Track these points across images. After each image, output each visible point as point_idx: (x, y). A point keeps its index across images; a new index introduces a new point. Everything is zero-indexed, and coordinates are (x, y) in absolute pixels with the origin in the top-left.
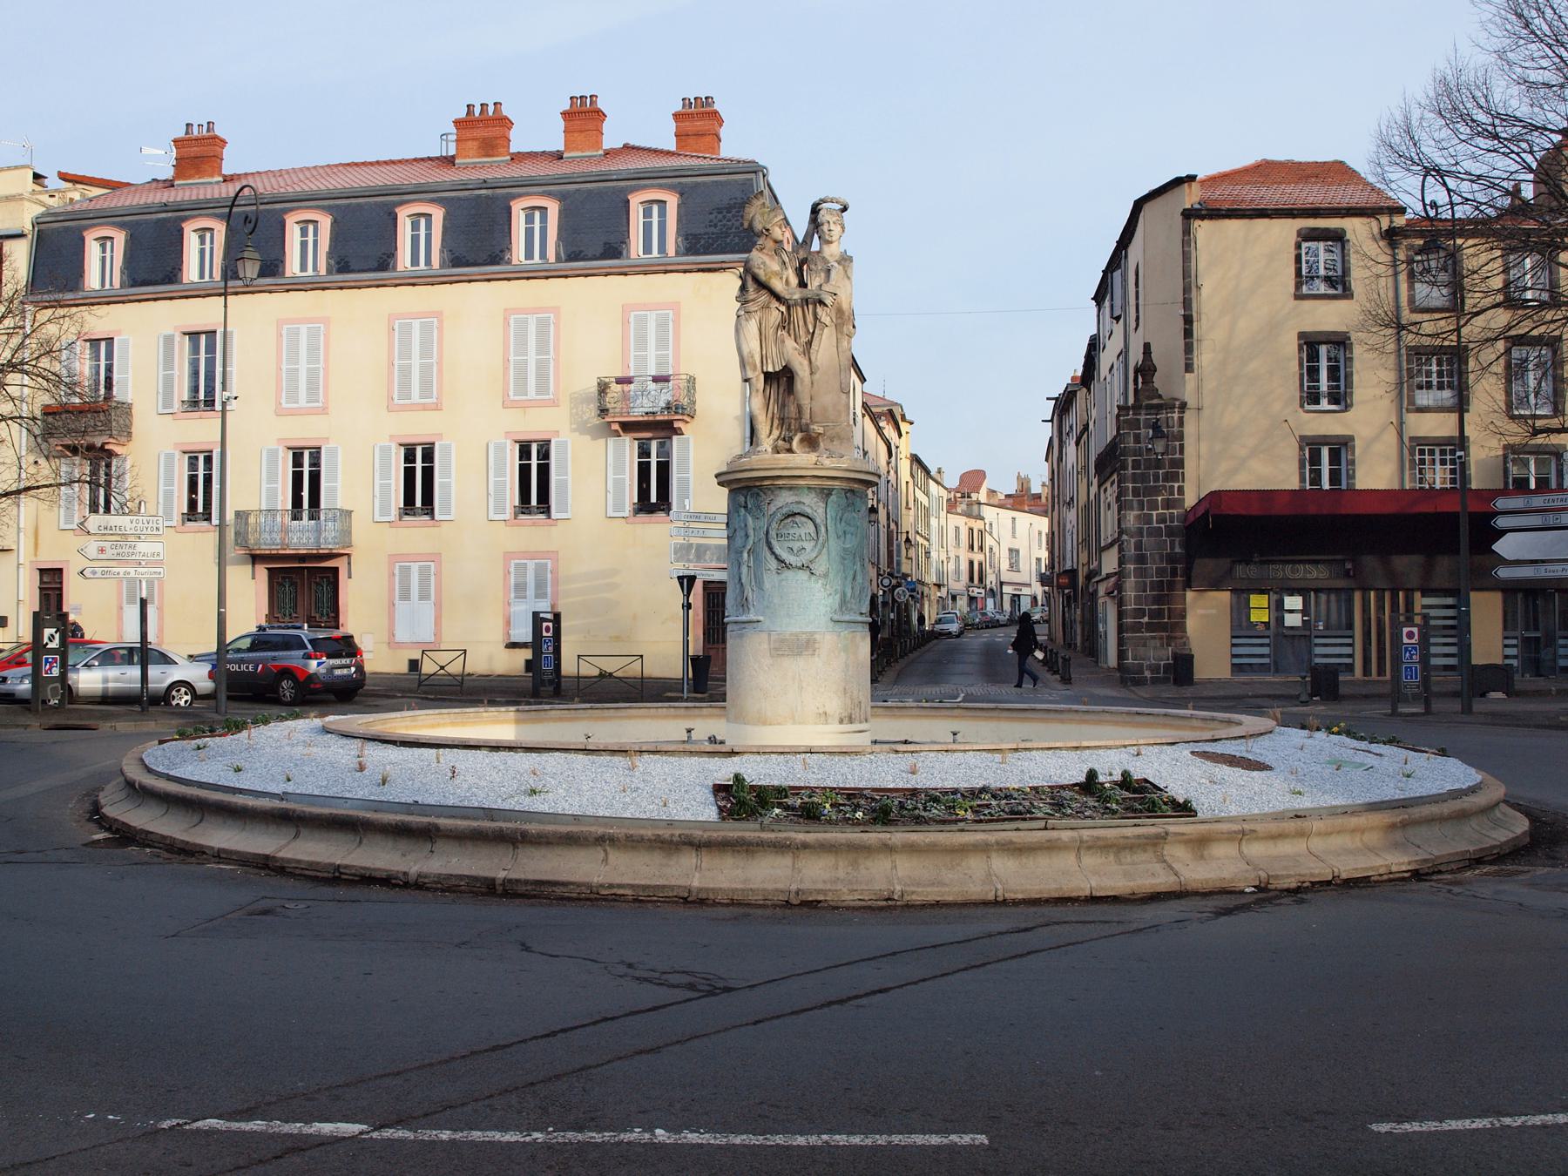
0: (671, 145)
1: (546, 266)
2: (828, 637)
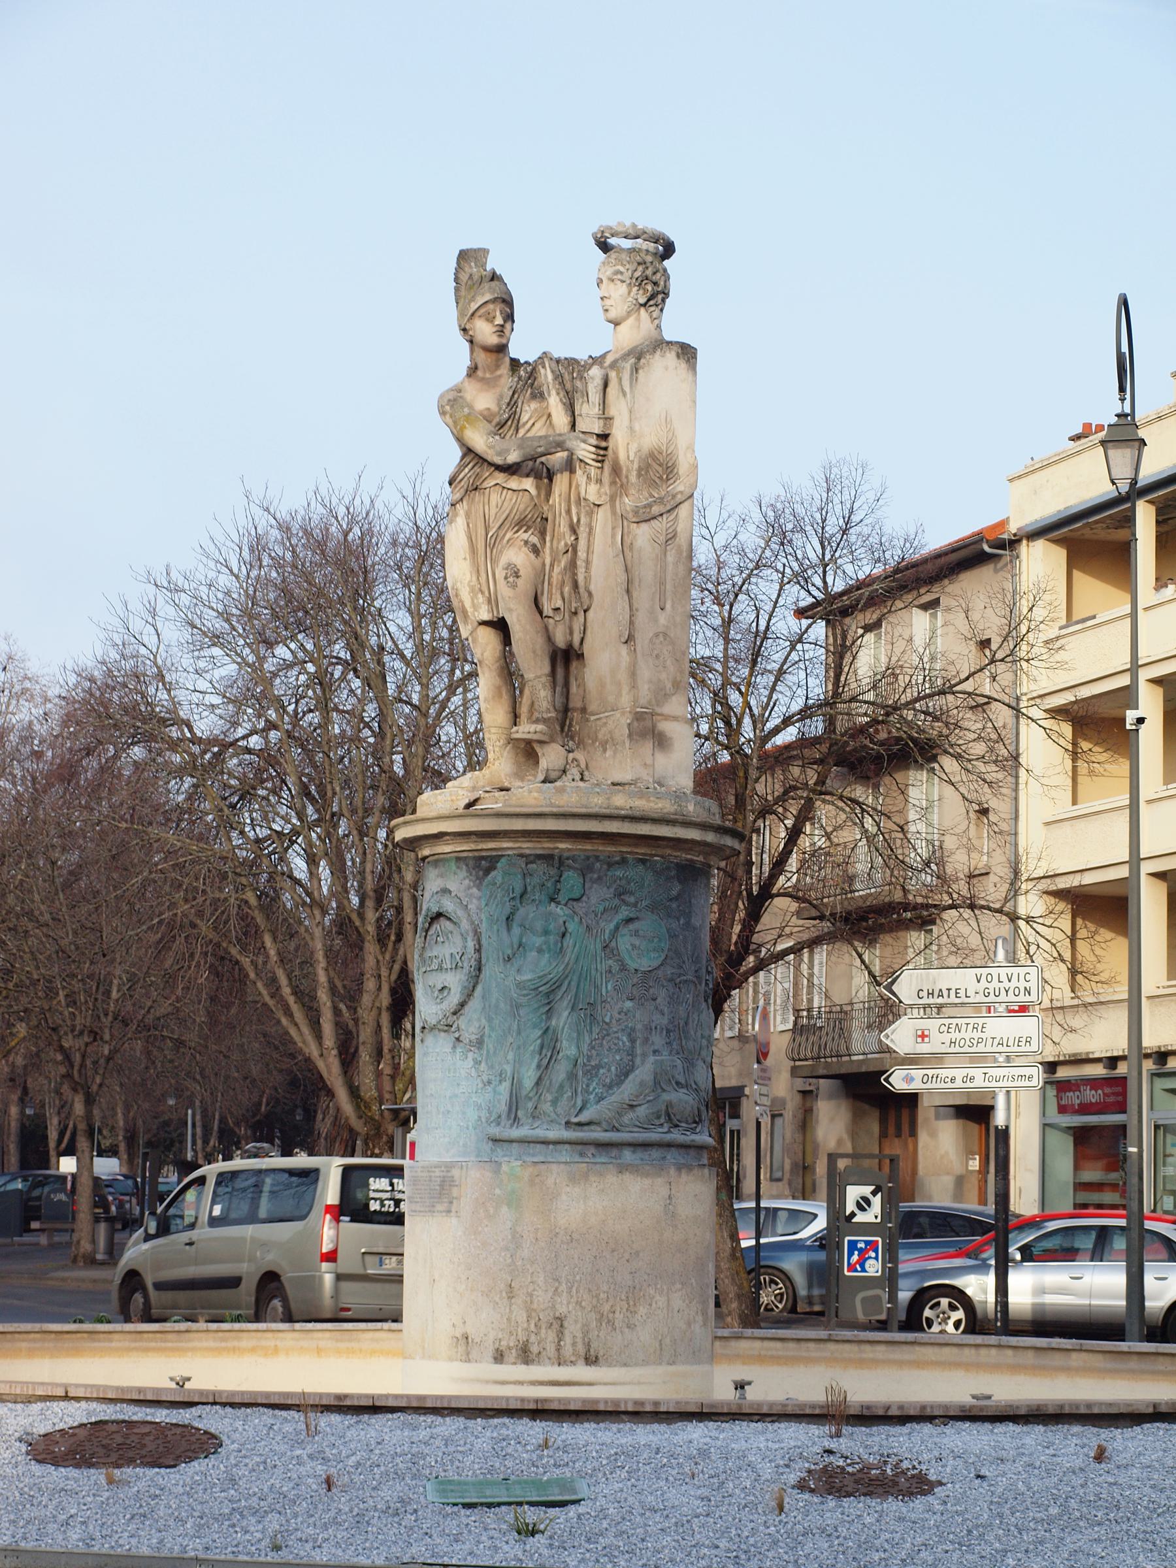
2: (474, 1174)
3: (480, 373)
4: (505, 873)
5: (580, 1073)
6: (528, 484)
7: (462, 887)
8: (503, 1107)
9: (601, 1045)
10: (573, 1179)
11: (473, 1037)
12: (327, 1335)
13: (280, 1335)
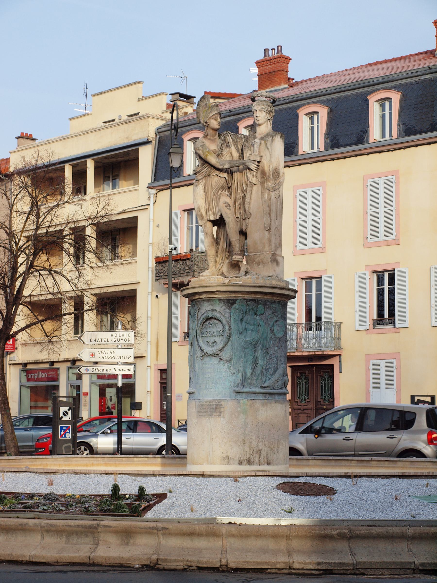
2: (230, 403)
3: (208, 137)
4: (239, 305)
5: (264, 371)
6: (226, 175)
7: (222, 309)
8: (239, 382)
9: (270, 362)
10: (263, 405)
11: (227, 359)
12: (62, 459)
13: (48, 460)
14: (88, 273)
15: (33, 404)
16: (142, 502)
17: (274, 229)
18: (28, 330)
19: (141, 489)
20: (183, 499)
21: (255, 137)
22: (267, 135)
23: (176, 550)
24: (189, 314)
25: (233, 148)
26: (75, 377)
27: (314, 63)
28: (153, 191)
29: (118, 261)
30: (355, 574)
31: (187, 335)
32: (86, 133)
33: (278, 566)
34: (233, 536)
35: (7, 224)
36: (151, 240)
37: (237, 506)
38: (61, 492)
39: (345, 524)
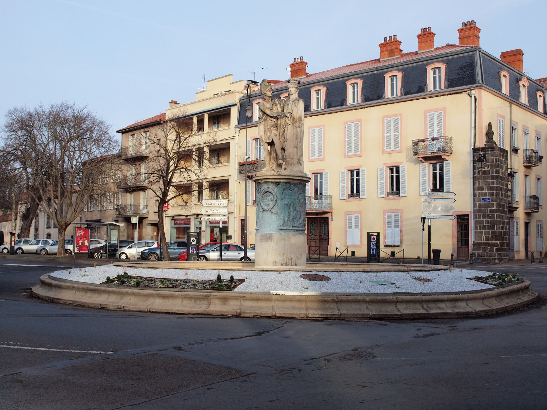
0: (457, 42)
1: (398, 98)
6: (275, 120)
8: (281, 224)
10: (293, 236)
14: (205, 171)
15: (177, 236)
16: (232, 284)
17: (299, 147)
18: (175, 199)
19: (232, 277)
20: (253, 282)
21: (290, 101)
22: (296, 100)
23: (250, 308)
24: (256, 190)
25: (278, 106)
26: (198, 223)
27: (319, 65)
28: (238, 130)
29: (220, 165)
30: (339, 320)
31: (255, 202)
32: (204, 100)
33: (301, 316)
34: (278, 300)
35: (164, 146)
36: (237, 154)
37: (280, 286)
38: (191, 279)
39: (335, 295)
